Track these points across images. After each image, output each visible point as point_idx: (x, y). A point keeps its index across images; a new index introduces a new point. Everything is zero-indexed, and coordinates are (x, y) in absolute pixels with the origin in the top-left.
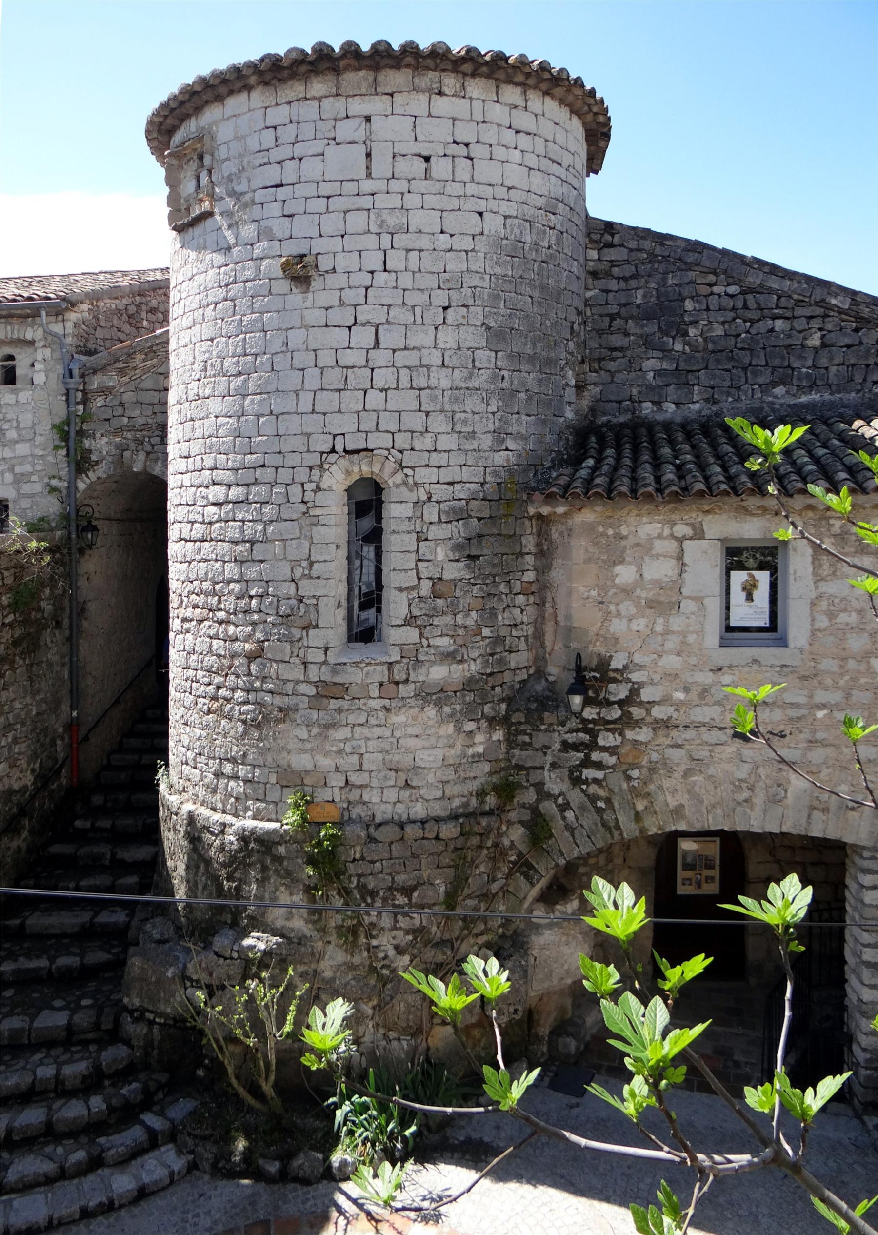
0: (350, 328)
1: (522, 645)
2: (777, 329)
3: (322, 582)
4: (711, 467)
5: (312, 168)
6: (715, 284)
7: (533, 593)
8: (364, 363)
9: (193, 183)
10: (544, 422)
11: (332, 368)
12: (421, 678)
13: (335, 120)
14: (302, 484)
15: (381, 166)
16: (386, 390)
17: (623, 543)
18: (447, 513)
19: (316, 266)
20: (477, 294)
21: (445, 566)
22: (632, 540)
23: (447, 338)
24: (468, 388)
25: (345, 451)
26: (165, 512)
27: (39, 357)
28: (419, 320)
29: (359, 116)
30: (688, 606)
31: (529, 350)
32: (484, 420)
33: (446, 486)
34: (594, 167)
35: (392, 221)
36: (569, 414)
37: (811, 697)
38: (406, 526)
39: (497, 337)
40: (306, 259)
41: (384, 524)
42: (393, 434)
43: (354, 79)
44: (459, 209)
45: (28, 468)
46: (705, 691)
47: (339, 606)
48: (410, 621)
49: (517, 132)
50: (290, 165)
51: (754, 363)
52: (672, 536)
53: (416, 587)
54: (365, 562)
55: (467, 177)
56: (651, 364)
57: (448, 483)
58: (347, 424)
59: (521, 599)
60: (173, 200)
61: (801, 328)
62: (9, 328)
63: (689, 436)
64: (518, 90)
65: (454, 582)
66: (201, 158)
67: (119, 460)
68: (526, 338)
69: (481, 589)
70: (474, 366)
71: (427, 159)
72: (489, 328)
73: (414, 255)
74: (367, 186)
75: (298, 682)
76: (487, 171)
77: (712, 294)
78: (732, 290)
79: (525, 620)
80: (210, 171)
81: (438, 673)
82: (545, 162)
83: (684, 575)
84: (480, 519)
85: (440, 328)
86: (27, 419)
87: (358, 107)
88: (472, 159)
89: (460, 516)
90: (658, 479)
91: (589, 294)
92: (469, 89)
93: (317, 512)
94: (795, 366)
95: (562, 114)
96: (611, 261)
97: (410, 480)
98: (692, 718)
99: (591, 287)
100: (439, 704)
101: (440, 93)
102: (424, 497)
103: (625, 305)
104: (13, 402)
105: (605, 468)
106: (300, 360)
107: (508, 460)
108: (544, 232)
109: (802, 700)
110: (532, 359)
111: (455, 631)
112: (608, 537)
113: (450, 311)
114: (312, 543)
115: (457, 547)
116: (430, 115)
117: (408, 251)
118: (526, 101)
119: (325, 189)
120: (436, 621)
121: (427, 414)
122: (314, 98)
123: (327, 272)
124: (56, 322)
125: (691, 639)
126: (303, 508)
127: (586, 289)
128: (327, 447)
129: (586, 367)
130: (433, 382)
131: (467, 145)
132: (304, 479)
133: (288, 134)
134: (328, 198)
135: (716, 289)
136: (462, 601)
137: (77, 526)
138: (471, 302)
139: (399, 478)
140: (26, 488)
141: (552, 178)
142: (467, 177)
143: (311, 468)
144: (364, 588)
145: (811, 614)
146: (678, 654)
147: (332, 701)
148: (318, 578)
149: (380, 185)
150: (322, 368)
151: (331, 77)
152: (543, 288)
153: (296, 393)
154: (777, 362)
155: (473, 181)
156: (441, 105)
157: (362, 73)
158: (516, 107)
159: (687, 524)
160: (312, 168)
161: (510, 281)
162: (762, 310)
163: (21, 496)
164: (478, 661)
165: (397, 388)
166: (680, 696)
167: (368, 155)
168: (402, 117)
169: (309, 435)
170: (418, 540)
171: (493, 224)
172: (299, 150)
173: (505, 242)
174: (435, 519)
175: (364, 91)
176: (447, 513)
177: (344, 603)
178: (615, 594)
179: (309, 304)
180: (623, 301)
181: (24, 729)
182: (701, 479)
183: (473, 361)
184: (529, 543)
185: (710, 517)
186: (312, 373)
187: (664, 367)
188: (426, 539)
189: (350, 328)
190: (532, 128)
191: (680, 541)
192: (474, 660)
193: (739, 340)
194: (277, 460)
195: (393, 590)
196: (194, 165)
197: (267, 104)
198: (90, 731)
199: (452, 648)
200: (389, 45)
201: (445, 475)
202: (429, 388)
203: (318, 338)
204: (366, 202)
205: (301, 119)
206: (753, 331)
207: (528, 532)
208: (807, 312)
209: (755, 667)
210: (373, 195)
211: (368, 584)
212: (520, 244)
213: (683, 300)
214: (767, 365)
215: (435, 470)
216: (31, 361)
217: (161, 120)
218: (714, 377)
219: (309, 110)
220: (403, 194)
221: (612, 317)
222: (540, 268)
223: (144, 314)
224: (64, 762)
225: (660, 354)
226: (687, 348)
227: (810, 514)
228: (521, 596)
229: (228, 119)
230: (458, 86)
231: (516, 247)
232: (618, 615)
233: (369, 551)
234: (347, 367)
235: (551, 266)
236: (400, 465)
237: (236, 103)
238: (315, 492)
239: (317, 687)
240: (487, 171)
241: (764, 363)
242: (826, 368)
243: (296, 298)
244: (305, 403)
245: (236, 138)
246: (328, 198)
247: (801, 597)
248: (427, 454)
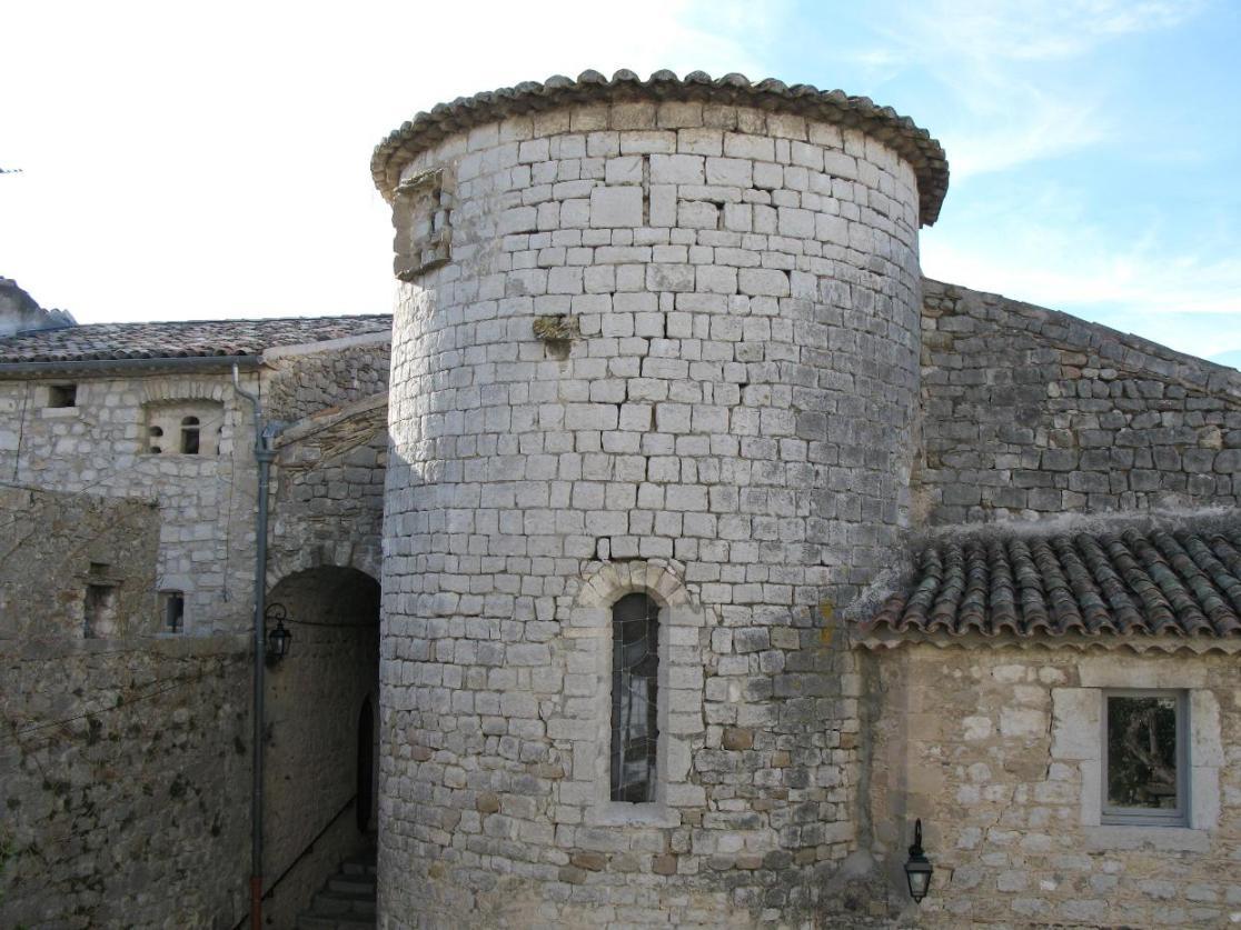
0: (619, 406)
1: (842, 815)
2: (1165, 424)
3: (578, 722)
4: (1087, 596)
5: (575, 213)
6: (1086, 366)
7: (855, 748)
8: (636, 448)
9: (427, 224)
10: (871, 530)
11: (596, 453)
12: (708, 851)
13: (606, 157)
14: (555, 598)
15: (662, 211)
16: (665, 484)
17: (976, 688)
18: (744, 643)
19: (578, 329)
20: (784, 369)
21: (741, 709)
22: (986, 685)
23: (745, 422)
24: (771, 486)
25: (611, 559)
26: (376, 623)
27: (228, 421)
28: (708, 399)
29: (636, 154)
30: (1059, 771)
31: (850, 440)
32: (793, 526)
33: (742, 608)
34: (929, 218)
35: (675, 277)
36: (903, 521)
37: (1223, 894)
38: (690, 657)
39: (809, 424)
40: (565, 320)
41: (661, 651)
42: (674, 539)
43: (627, 110)
44: (760, 266)
45: (209, 555)
46: (1081, 883)
47: (600, 753)
48: (695, 776)
49: (833, 177)
50: (546, 208)
51: (1138, 464)
52: (1038, 682)
53: (702, 736)
54: (635, 700)
55: (770, 229)
56: (1006, 461)
57: (745, 604)
58: (614, 524)
59: (840, 755)
60: (399, 244)
61: (1196, 424)
62: (194, 385)
63: (1058, 553)
64: (833, 129)
65: (752, 730)
66: (437, 195)
67: (318, 552)
68: (846, 425)
69: (787, 741)
70: (779, 458)
72: (799, 411)
73: (703, 320)
75: (546, 847)
76: (794, 221)
77: (1082, 377)
78: (1107, 374)
79: (845, 781)
80: (448, 211)
81: (730, 845)
82: (869, 215)
83: (1054, 732)
84: (786, 651)
85: (736, 409)
86: (209, 496)
87: (633, 143)
88: (776, 207)
89: (759, 647)
90: (1019, 608)
91: (926, 371)
92: (772, 127)
93: (573, 634)
94: (1189, 470)
95: (888, 158)
96: (954, 332)
97: (696, 600)
98: (1066, 914)
99: (928, 362)
100: (732, 886)
101: (736, 130)
102: (713, 621)
103: (971, 387)
104: (193, 474)
105: (950, 594)
106: (554, 441)
107: (823, 578)
108: (869, 297)
109: (1212, 897)
110: (853, 452)
111: (752, 793)
112: (954, 680)
113: (748, 389)
114: (566, 673)
115: (755, 686)
116: (723, 155)
117: (695, 313)
118: (843, 142)
119: (592, 237)
120: (728, 779)
121: (719, 516)
122: (580, 132)
123: (591, 336)
124: (251, 380)
125: (1064, 813)
126: (555, 627)
127: (922, 364)
128: (587, 552)
129: (923, 462)
130: (726, 476)
131: (770, 191)
132: (557, 590)
133: (547, 172)
134: (595, 248)
135: (1086, 372)
136: (762, 754)
137: (265, 630)
138: (775, 378)
139: (681, 595)
140: (206, 580)
141: (877, 232)
142: (770, 229)
143: (566, 577)
144: (633, 734)
145: (1221, 787)
146: (1047, 832)
147: (590, 873)
148: (574, 717)
149: (662, 235)
150: (583, 454)
151: (600, 108)
152: (869, 365)
153: (549, 482)
154: (1165, 465)
156: (737, 144)
157: (640, 106)
158: (830, 148)
159: (1057, 668)
160: (575, 213)
161: (825, 355)
162: (1146, 399)
163: (200, 588)
164: (783, 832)
165: (679, 482)
166: (1050, 885)
167: (646, 199)
168: (688, 160)
169: (565, 536)
170: (706, 675)
171: (803, 285)
172: (559, 191)
173: (818, 307)
174: (727, 648)
175: (641, 126)
176: (744, 643)
177: (607, 750)
178: (965, 752)
179: (567, 373)
180: (970, 382)
181: (195, 878)
182: (1076, 611)
183: (779, 452)
184: (852, 684)
185: (1088, 658)
186: (571, 459)
187: (1024, 465)
188: (716, 675)
189: (619, 406)
190: (852, 173)
191: (1049, 688)
192: (778, 831)
193: (1118, 435)
194: (524, 565)
195: (671, 738)
196: (429, 204)
197: (522, 138)
198: (275, 885)
199: (748, 815)
200: (674, 75)
201: (742, 594)
202: (721, 483)
203: (581, 416)
204: (643, 254)
205: (563, 156)
206: (1134, 425)
207: (849, 669)
208: (1205, 404)
209: (1148, 852)
210: (651, 246)
211: (639, 727)
212: (839, 311)
213: (1046, 384)
214: (1154, 468)
215: (728, 587)
216: (217, 425)
217: (391, 151)
218: (1087, 480)
219: (573, 146)
220: (689, 246)
221: (956, 401)
222: (864, 339)
223: (354, 372)
224: (243, 921)
225: (1018, 449)
226: (1052, 442)
227: (1216, 660)
228: (840, 752)
229: (473, 153)
230: (758, 122)
231: (832, 314)
232: (968, 780)
233: (640, 687)
234: (615, 454)
235: (878, 337)
236: (683, 579)
237: (484, 136)
238: (571, 609)
239: (570, 854)
240: (794, 221)
241: (1150, 466)
242: (1230, 475)
243: (552, 366)
244: (561, 495)
245: (482, 175)
246: (595, 248)
247: (1206, 764)
248: (717, 567)
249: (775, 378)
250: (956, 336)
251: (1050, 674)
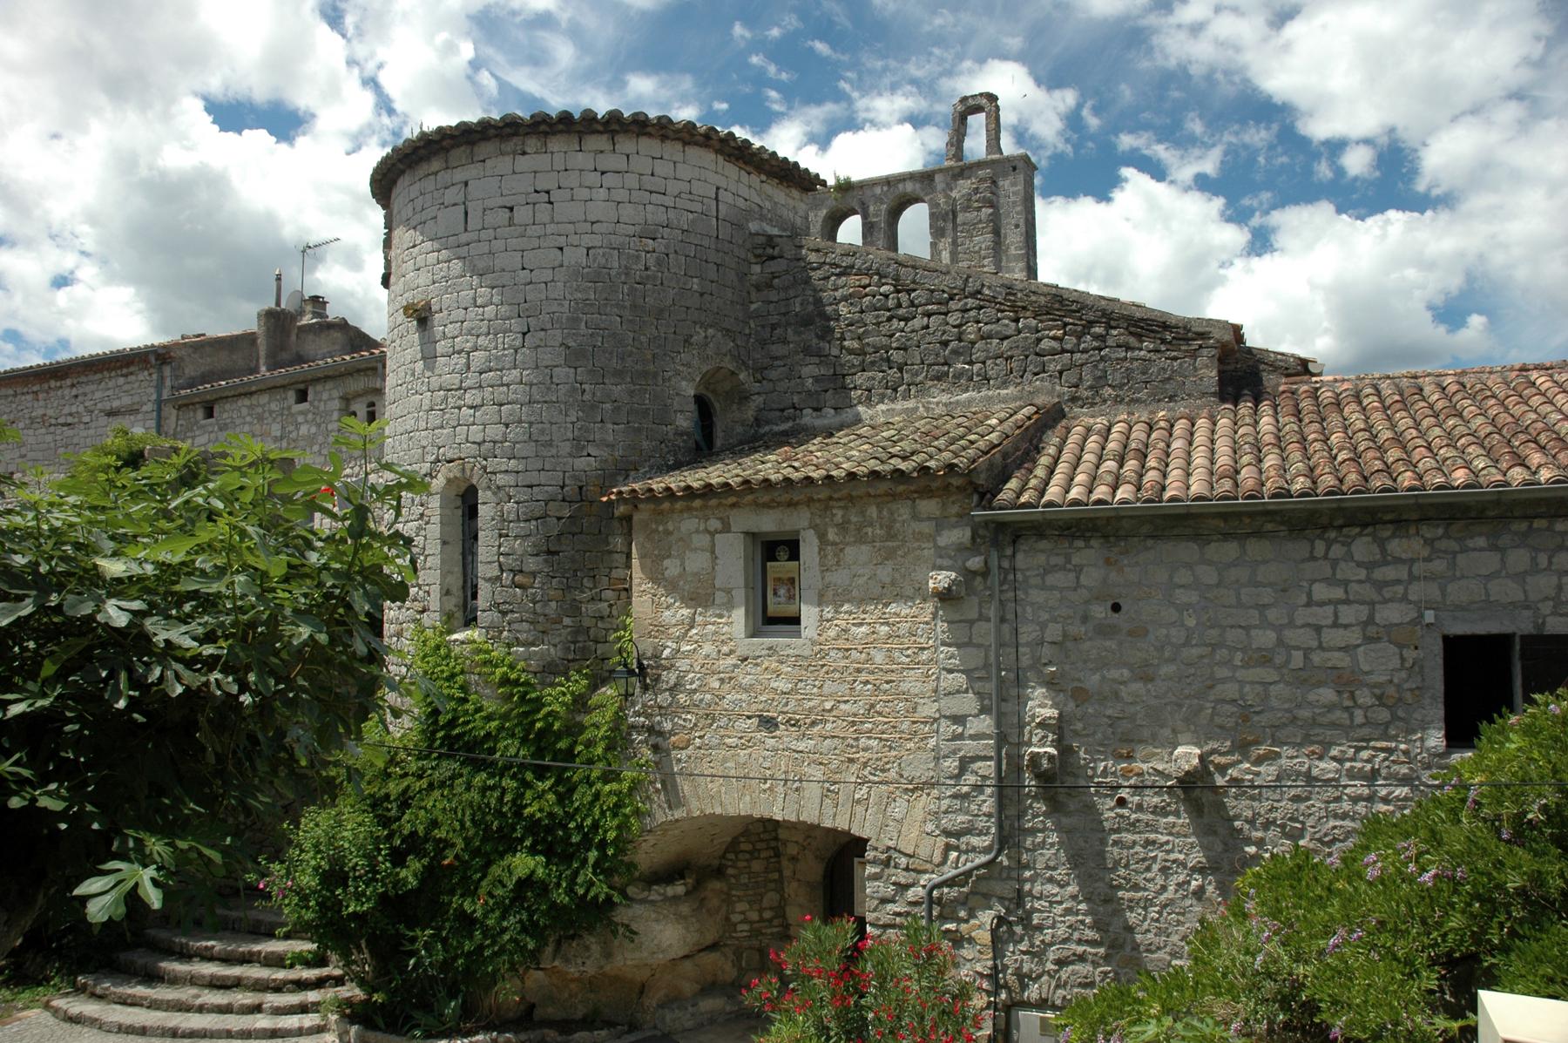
15: (473, 223)
39: (574, 357)
52: (707, 531)
53: (499, 578)
55: (547, 219)
71: (511, 209)
74: (464, 238)
76: (565, 210)
110: (619, 374)
138: (549, 326)
142: (547, 219)
155: (552, 221)
156: (523, 163)
171: (575, 256)
221: (774, 327)
249: (549, 326)
250: (774, 276)
251: (714, 524)
